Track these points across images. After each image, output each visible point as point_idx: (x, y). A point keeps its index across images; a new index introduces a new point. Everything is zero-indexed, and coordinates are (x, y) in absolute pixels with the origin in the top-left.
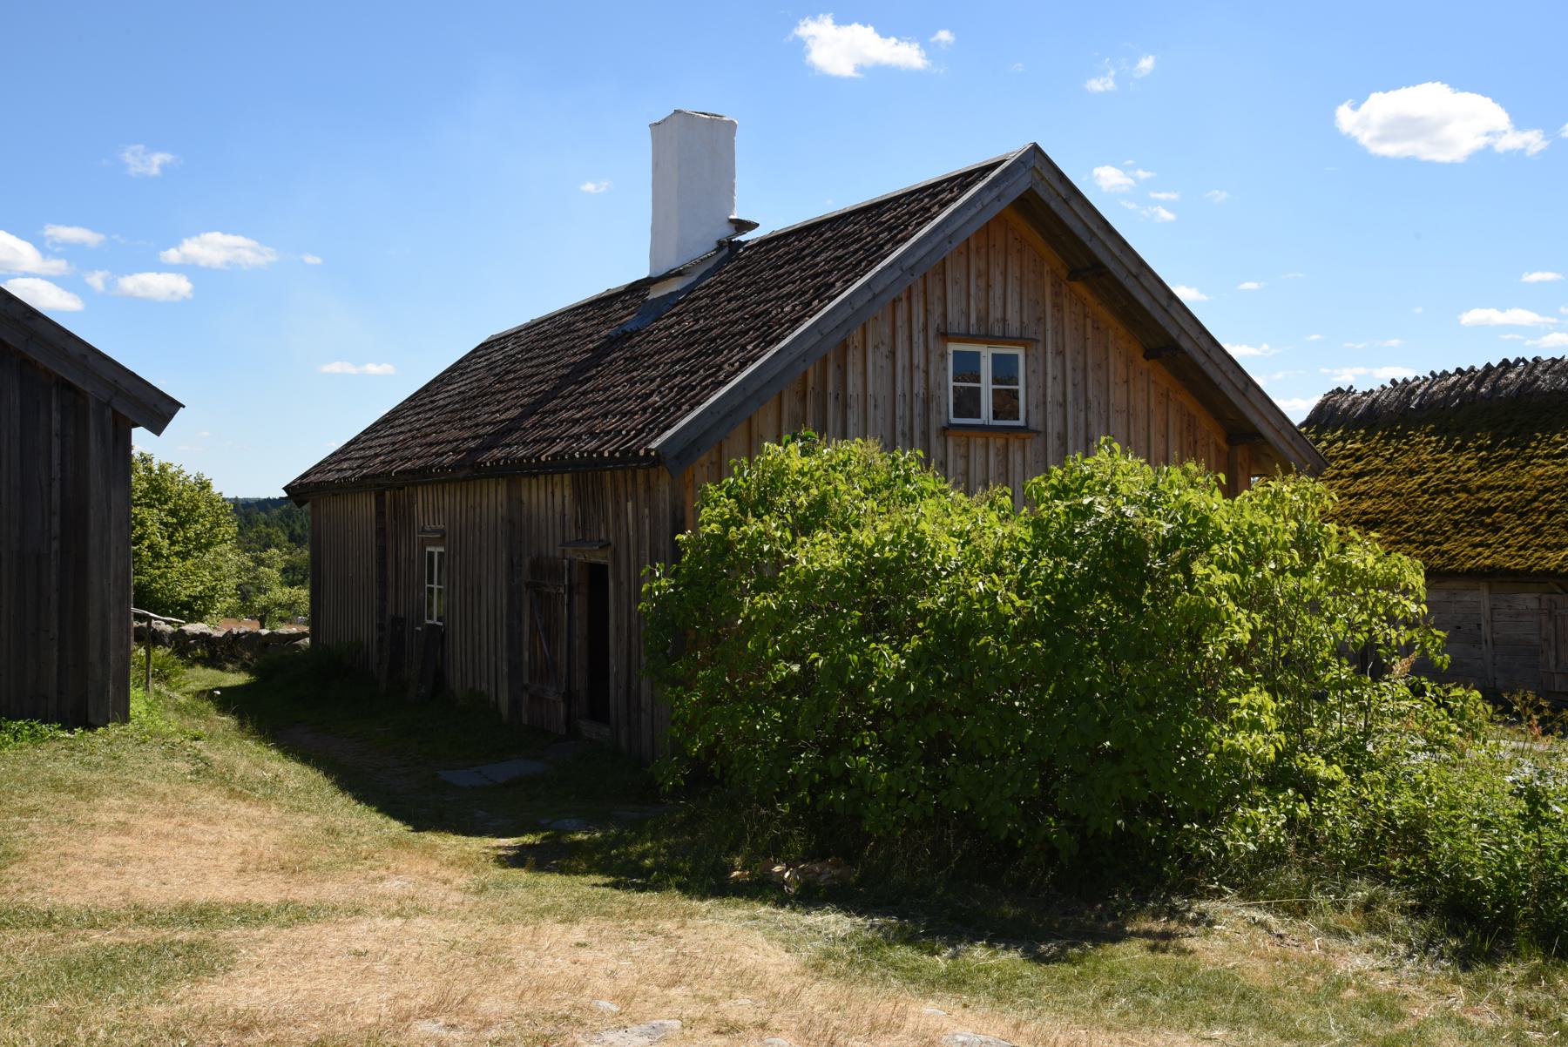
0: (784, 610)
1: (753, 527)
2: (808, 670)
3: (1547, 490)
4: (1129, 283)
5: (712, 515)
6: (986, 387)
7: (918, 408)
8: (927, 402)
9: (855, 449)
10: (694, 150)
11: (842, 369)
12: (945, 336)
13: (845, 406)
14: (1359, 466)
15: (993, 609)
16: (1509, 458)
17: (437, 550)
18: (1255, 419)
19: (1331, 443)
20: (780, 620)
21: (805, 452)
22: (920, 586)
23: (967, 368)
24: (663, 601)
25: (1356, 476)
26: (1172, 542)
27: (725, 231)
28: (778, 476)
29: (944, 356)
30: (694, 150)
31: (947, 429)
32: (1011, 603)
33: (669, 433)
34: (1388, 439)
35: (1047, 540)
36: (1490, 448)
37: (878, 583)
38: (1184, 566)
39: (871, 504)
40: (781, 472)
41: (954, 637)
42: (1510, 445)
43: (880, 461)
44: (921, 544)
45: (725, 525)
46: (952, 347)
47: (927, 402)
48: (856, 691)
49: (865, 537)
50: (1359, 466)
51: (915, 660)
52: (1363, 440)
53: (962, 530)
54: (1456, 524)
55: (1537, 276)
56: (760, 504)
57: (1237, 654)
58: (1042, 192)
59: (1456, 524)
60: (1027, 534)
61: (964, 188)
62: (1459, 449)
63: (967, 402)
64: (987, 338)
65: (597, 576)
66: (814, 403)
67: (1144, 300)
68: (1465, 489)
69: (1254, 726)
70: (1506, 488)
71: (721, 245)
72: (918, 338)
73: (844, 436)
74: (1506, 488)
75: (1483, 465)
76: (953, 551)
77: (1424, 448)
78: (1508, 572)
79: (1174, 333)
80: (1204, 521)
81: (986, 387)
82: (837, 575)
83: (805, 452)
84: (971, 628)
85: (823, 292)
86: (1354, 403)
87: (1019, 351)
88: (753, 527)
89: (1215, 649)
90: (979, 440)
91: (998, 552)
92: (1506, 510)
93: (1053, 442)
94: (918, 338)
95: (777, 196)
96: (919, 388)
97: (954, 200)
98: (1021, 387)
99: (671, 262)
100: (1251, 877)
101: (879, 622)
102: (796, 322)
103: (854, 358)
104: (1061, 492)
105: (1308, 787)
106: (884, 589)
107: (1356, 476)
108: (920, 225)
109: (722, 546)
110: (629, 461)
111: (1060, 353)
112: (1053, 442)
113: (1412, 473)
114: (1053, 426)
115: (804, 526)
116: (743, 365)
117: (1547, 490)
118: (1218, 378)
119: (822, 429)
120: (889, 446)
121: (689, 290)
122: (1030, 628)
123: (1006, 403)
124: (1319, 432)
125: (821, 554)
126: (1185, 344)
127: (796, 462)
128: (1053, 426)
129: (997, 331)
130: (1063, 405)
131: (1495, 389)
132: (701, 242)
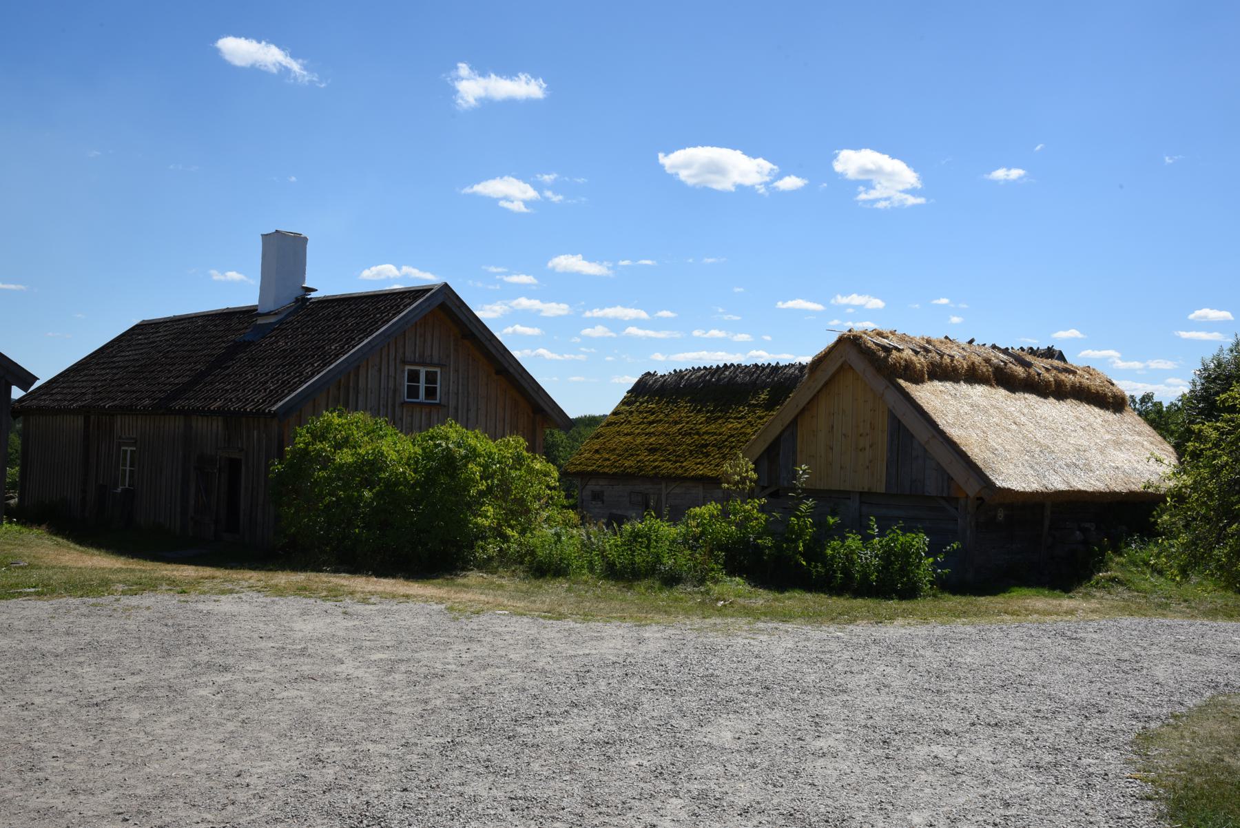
0: (329, 477)
1: (319, 446)
2: (339, 498)
3: (732, 436)
4: (487, 343)
5: (302, 438)
6: (422, 385)
7: (390, 394)
8: (395, 391)
9: (359, 415)
10: (284, 251)
11: (357, 375)
12: (404, 362)
13: (357, 393)
14: (652, 418)
15: (405, 478)
16: (719, 417)
17: (129, 449)
18: (542, 404)
19: (641, 403)
20: (329, 480)
21: (339, 416)
22: (381, 470)
23: (414, 376)
24: (280, 474)
25: (651, 423)
26: (466, 457)
27: (300, 293)
28: (328, 426)
29: (403, 371)
30: (284, 251)
31: (403, 404)
32: (410, 474)
33: (280, 404)
34: (668, 403)
35: (428, 455)
36: (712, 412)
37: (366, 468)
38: (466, 465)
39: (366, 438)
40: (330, 424)
41: (391, 486)
42: (721, 411)
43: (370, 422)
44: (382, 454)
45: (307, 444)
46: (407, 368)
47: (395, 391)
48: (356, 506)
49: (362, 451)
50: (652, 418)
51: (376, 495)
52: (657, 403)
53: (397, 448)
54: (691, 452)
55: (574, 379)
56: (323, 437)
57: (481, 494)
58: (448, 303)
59: (691, 452)
60: (419, 451)
61: (415, 299)
62: (699, 411)
63: (413, 392)
64: (423, 364)
65: (234, 466)
66: (343, 394)
67: (494, 351)
68: (698, 433)
69: (488, 515)
70: (715, 434)
71: (297, 300)
72: (392, 363)
73: (356, 410)
74: (715, 434)
75: (708, 421)
76: (394, 456)
77: (684, 410)
78: (709, 478)
79: (506, 365)
80: (475, 450)
81: (422, 385)
82: (350, 465)
83: (339, 416)
84: (397, 484)
85: (350, 343)
86: (656, 381)
87: (438, 370)
88: (319, 446)
89: (473, 492)
90: (409, 411)
91: (409, 458)
92: (714, 445)
93: (451, 410)
94: (392, 363)
95: (327, 279)
96: (391, 385)
97: (410, 304)
98: (438, 386)
99: (270, 306)
100: (485, 565)
101: (369, 484)
102: (337, 356)
103: (362, 371)
104: (432, 438)
105: (506, 538)
106: (370, 468)
107: (651, 423)
108: (395, 315)
109: (305, 452)
110: (259, 414)
111: (457, 371)
112: (451, 410)
113: (676, 423)
114: (452, 404)
115: (338, 446)
116: (312, 375)
117: (732, 436)
118: (526, 385)
119: (346, 405)
120: (373, 416)
121: (280, 322)
122: (417, 483)
123: (431, 392)
124: (637, 397)
125: (345, 457)
126: (511, 370)
127: (336, 421)
128: (452, 404)
129: (428, 361)
130: (457, 394)
131: (718, 380)
132: (287, 299)
